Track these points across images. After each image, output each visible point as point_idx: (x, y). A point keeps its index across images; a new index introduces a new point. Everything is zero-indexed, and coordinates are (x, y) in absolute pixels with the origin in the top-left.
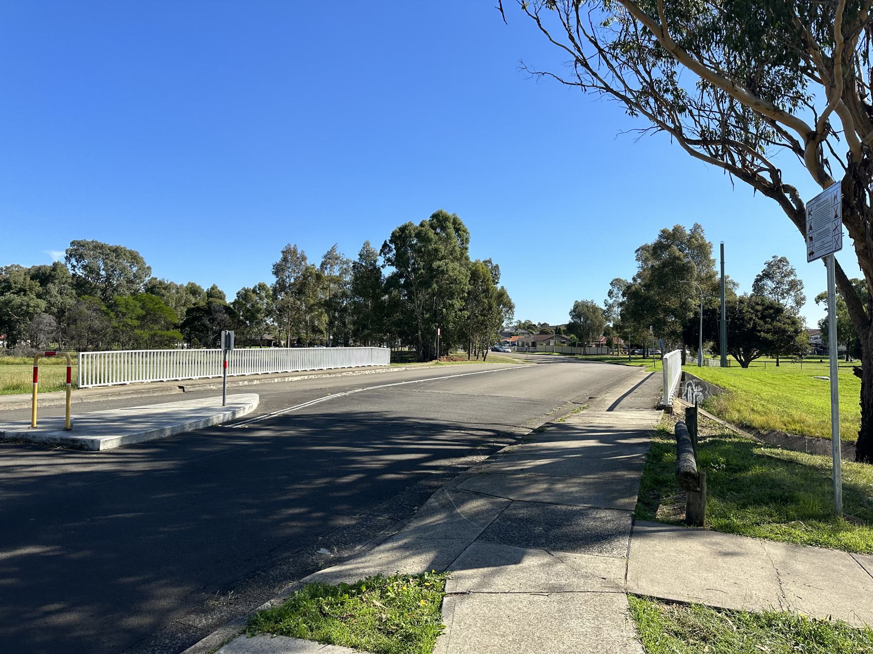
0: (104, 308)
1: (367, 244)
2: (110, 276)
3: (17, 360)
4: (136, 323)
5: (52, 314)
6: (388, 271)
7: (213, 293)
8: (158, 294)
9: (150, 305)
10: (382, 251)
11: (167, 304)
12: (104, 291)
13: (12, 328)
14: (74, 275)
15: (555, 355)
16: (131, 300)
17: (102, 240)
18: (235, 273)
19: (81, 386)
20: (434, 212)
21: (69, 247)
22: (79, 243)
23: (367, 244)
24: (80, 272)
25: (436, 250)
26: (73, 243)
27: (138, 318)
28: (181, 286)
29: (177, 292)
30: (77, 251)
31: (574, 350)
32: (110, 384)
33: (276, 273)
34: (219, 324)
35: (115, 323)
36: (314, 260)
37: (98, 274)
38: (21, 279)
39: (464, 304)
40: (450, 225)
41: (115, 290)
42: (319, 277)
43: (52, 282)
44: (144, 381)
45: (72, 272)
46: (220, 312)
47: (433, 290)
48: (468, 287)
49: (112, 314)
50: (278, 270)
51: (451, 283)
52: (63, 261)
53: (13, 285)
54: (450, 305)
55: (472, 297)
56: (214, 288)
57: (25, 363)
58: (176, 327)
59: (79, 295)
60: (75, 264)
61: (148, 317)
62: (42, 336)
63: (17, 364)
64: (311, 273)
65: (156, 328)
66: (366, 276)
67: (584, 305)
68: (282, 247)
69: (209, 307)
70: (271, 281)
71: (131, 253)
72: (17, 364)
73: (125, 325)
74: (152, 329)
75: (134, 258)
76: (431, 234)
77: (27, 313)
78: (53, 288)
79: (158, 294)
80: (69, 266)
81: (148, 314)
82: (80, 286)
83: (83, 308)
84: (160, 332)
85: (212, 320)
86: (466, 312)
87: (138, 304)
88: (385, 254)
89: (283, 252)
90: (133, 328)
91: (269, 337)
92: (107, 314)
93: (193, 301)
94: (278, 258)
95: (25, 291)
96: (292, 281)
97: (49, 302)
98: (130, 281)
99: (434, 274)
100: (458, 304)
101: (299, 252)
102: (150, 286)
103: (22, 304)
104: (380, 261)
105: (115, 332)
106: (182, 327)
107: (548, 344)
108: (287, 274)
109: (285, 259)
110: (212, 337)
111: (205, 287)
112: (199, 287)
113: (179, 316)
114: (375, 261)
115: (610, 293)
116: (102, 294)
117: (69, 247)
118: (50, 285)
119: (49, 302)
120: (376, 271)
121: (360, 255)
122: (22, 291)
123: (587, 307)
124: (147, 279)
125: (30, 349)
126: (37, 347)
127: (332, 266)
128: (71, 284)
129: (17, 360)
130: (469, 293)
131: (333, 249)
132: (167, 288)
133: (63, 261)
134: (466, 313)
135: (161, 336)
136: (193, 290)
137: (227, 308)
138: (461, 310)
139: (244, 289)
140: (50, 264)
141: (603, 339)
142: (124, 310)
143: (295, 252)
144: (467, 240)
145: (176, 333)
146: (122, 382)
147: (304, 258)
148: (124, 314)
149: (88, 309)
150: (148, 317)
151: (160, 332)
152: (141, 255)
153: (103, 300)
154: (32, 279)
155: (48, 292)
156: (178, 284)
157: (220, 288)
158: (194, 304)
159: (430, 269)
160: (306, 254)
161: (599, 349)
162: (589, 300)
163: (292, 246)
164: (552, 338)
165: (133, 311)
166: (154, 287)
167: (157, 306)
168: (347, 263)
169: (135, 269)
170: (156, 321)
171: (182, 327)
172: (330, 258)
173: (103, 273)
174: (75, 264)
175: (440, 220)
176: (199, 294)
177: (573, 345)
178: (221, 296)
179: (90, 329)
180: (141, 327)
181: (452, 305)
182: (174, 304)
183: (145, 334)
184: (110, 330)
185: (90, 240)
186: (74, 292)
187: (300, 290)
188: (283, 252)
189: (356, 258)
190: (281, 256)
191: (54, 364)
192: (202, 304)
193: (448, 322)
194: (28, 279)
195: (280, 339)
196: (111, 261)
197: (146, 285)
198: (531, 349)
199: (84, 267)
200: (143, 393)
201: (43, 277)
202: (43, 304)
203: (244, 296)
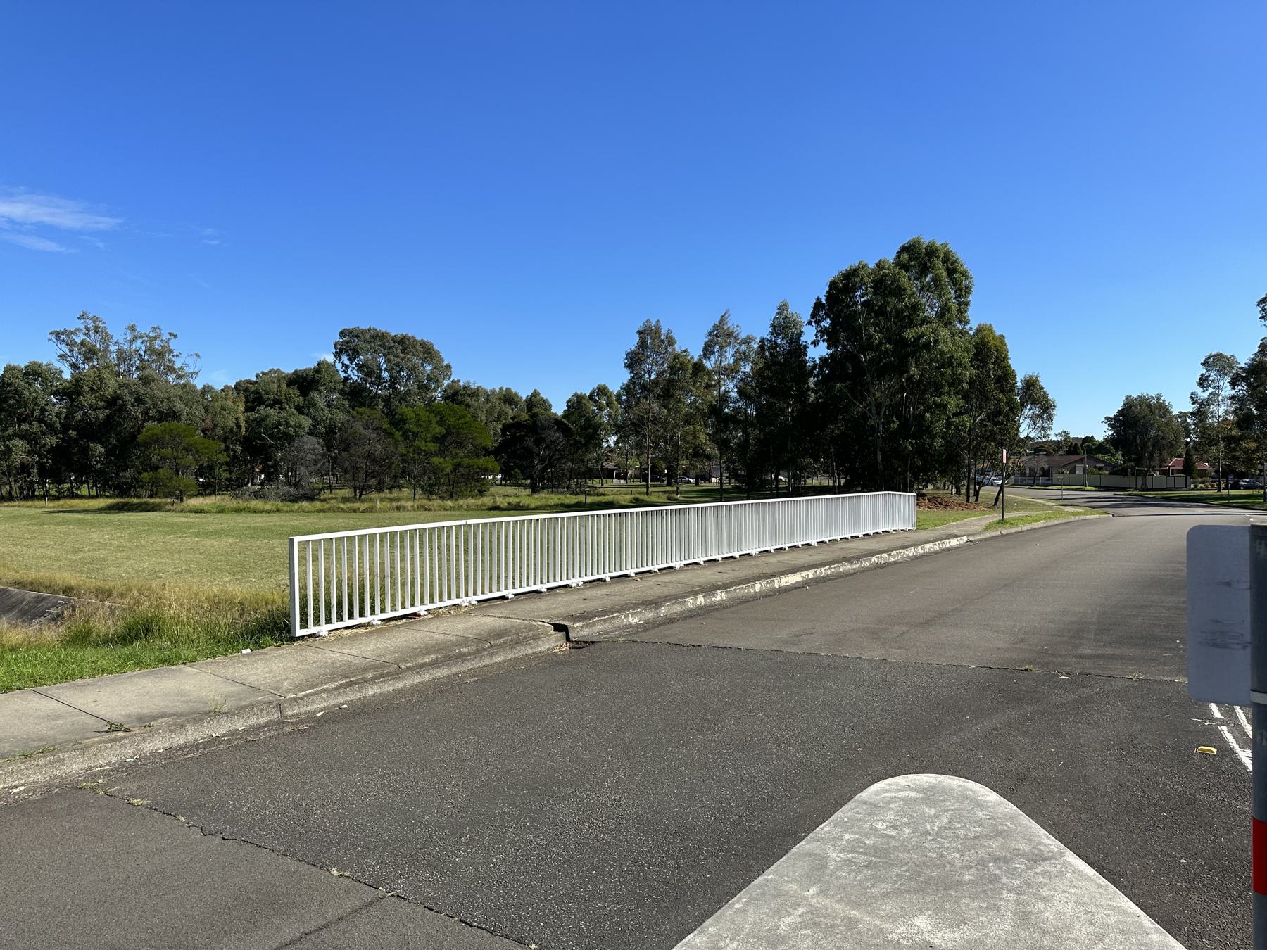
0: (386, 426)
1: (783, 307)
2: (396, 378)
3: (269, 506)
4: (433, 447)
5: (319, 435)
6: (817, 352)
7: (535, 403)
8: (461, 403)
9: (451, 421)
10: (813, 316)
11: (475, 417)
12: (387, 400)
13: (268, 457)
14: (346, 379)
15: (1090, 492)
16: (424, 414)
17: (381, 328)
18: (567, 367)
19: (299, 632)
20: (905, 241)
21: (337, 338)
22: (351, 332)
23: (783, 307)
24: (355, 376)
25: (915, 308)
26: (342, 334)
27: (436, 439)
28: (493, 391)
29: (488, 401)
30: (350, 344)
31: (1123, 481)
32: (377, 618)
33: (630, 366)
34: (547, 446)
35: (402, 449)
36: (691, 344)
37: (380, 377)
38: (275, 387)
39: (962, 403)
40: (938, 263)
41: (403, 399)
42: (698, 368)
43: (316, 389)
44: (463, 601)
45: (343, 375)
46: (549, 428)
47: (910, 378)
48: (969, 373)
49: (397, 434)
50: (633, 361)
51: (943, 366)
52: (330, 359)
53: (265, 396)
54: (937, 405)
55: (976, 393)
56: (535, 395)
57: (278, 511)
58: (488, 453)
59: (352, 407)
60: (347, 362)
61: (448, 439)
62: (302, 469)
63: (268, 512)
64: (682, 363)
65: (462, 454)
66: (779, 363)
67: (1143, 402)
68: (639, 326)
69: (534, 422)
70: (617, 379)
71: (423, 344)
72: (268, 512)
73: (418, 450)
74: (454, 457)
75: (428, 352)
76: (903, 278)
77: (286, 434)
78: (319, 399)
79: (461, 403)
80: (339, 366)
81: (449, 433)
82: (355, 394)
83: (358, 426)
84: (466, 461)
85: (539, 442)
86: (966, 418)
87: (434, 420)
88: (817, 323)
89: (640, 333)
90: (429, 455)
91: (610, 465)
92: (389, 434)
93: (511, 414)
94: (632, 342)
95: (281, 403)
96: (653, 377)
97: (314, 418)
98: (423, 387)
99: (906, 351)
100: (953, 403)
101: (664, 331)
102: (450, 392)
103: (279, 423)
104: (809, 334)
105: (404, 461)
106: (496, 452)
107: (1073, 471)
108: (646, 367)
109: (642, 345)
110: (539, 467)
111: (524, 394)
112: (516, 394)
113: (492, 435)
114: (799, 335)
115: (1203, 382)
116: (385, 406)
117: (337, 338)
118: (314, 394)
119: (314, 418)
120: (798, 350)
121: (773, 326)
122: (277, 403)
123: (1149, 406)
124: (446, 382)
125: (286, 488)
126: (296, 485)
127: (721, 348)
128: (342, 392)
129: (268, 507)
130: (971, 383)
131: (723, 320)
132: (474, 394)
133: (330, 359)
134: (967, 420)
135: (469, 466)
136: (509, 398)
137: (558, 422)
138: (955, 415)
139: (575, 395)
140: (312, 365)
141: (1174, 463)
142: (415, 429)
143: (658, 331)
144: (968, 290)
145: (490, 461)
146: (410, 610)
147: (671, 342)
148: (415, 435)
149: (361, 425)
150: (448, 439)
151: (466, 461)
152: (436, 347)
153: (387, 415)
154: (288, 385)
155: (311, 404)
156: (488, 388)
157: (543, 395)
158: (513, 418)
159: (902, 343)
160: (675, 335)
161: (1170, 480)
162: (1153, 394)
163: (654, 323)
164: (1081, 461)
165: (427, 429)
166: (456, 393)
167: (462, 421)
168: (747, 341)
169: (429, 368)
170: (460, 445)
171: (496, 452)
172: (719, 336)
173: (385, 374)
174: (347, 362)
175: (918, 258)
176: (516, 404)
177: (1122, 472)
178: (546, 405)
179: (371, 458)
180: (441, 453)
181: (943, 407)
182: (484, 418)
183: (447, 464)
184: (396, 460)
185: (365, 327)
186: (346, 403)
187: (667, 390)
188: (640, 333)
189: (766, 332)
190: (637, 338)
191: (319, 511)
192: (524, 417)
193: (933, 437)
194: (284, 386)
195: (627, 468)
196: (397, 356)
197: (445, 391)
198: (1042, 480)
199: (360, 367)
200: (463, 657)
201: (305, 382)
202: (307, 422)
203: (576, 404)
